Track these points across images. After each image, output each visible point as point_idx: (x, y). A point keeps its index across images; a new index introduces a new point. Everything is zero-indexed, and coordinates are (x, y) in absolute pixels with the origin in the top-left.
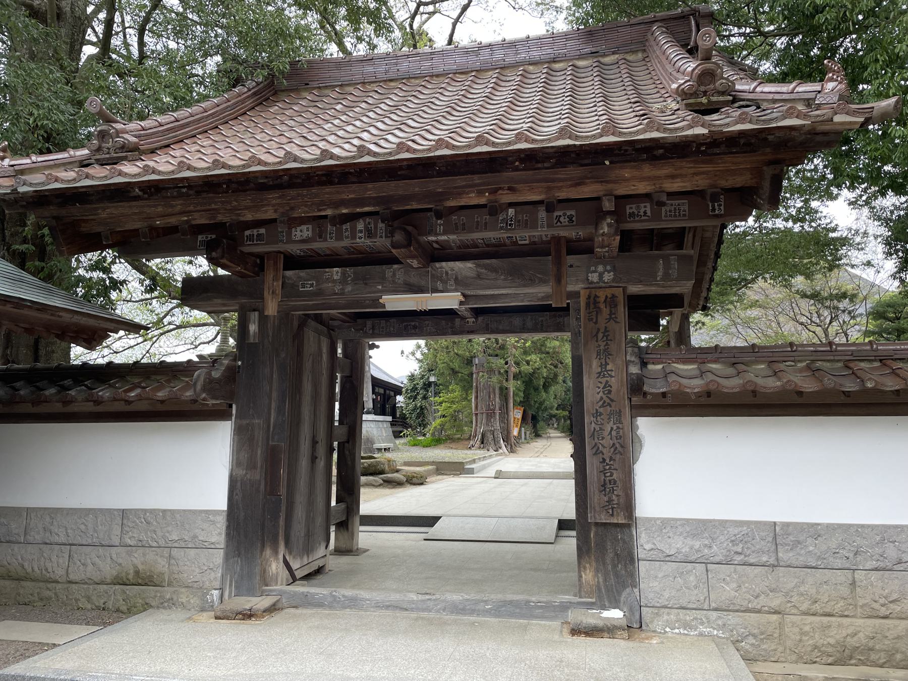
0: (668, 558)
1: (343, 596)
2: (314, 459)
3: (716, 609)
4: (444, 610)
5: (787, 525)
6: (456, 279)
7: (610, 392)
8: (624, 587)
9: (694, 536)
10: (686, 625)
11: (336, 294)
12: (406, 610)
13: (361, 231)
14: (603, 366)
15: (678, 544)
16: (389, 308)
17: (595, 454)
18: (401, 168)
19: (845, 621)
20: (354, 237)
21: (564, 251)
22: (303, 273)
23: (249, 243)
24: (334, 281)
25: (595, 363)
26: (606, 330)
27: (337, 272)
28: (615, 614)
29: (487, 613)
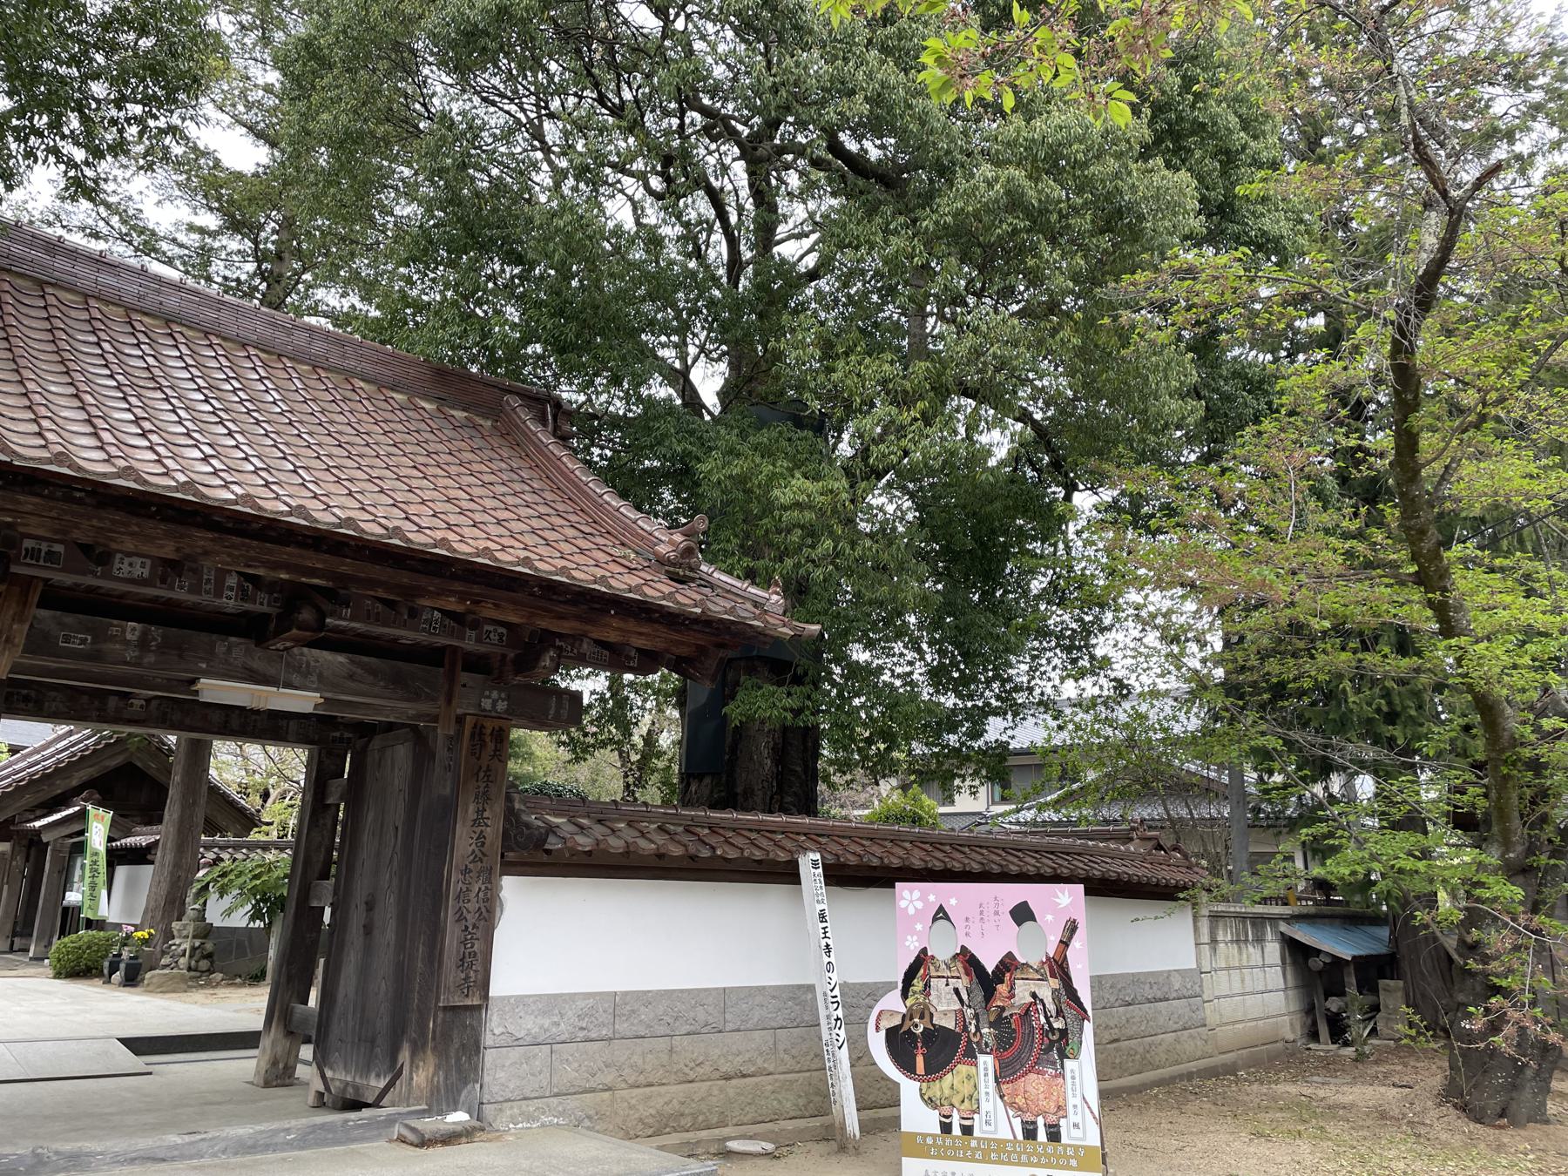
0: (517, 1042)
1: (57, 1153)
2: (368, 930)
3: (556, 1095)
4: (224, 1152)
5: (626, 993)
6: (320, 676)
7: (483, 844)
8: (466, 1084)
9: (544, 1013)
10: (529, 1118)
11: (126, 663)
12: (164, 1160)
13: (231, 589)
14: (480, 812)
15: (529, 1025)
16: (206, 697)
17: (458, 921)
18: (412, 558)
19: (662, 1089)
20: (219, 594)
21: (459, 667)
22: (70, 619)
23: (28, 561)
24: (126, 643)
25: (472, 808)
26: (488, 769)
27: (134, 629)
28: (459, 1117)
29: (290, 1145)
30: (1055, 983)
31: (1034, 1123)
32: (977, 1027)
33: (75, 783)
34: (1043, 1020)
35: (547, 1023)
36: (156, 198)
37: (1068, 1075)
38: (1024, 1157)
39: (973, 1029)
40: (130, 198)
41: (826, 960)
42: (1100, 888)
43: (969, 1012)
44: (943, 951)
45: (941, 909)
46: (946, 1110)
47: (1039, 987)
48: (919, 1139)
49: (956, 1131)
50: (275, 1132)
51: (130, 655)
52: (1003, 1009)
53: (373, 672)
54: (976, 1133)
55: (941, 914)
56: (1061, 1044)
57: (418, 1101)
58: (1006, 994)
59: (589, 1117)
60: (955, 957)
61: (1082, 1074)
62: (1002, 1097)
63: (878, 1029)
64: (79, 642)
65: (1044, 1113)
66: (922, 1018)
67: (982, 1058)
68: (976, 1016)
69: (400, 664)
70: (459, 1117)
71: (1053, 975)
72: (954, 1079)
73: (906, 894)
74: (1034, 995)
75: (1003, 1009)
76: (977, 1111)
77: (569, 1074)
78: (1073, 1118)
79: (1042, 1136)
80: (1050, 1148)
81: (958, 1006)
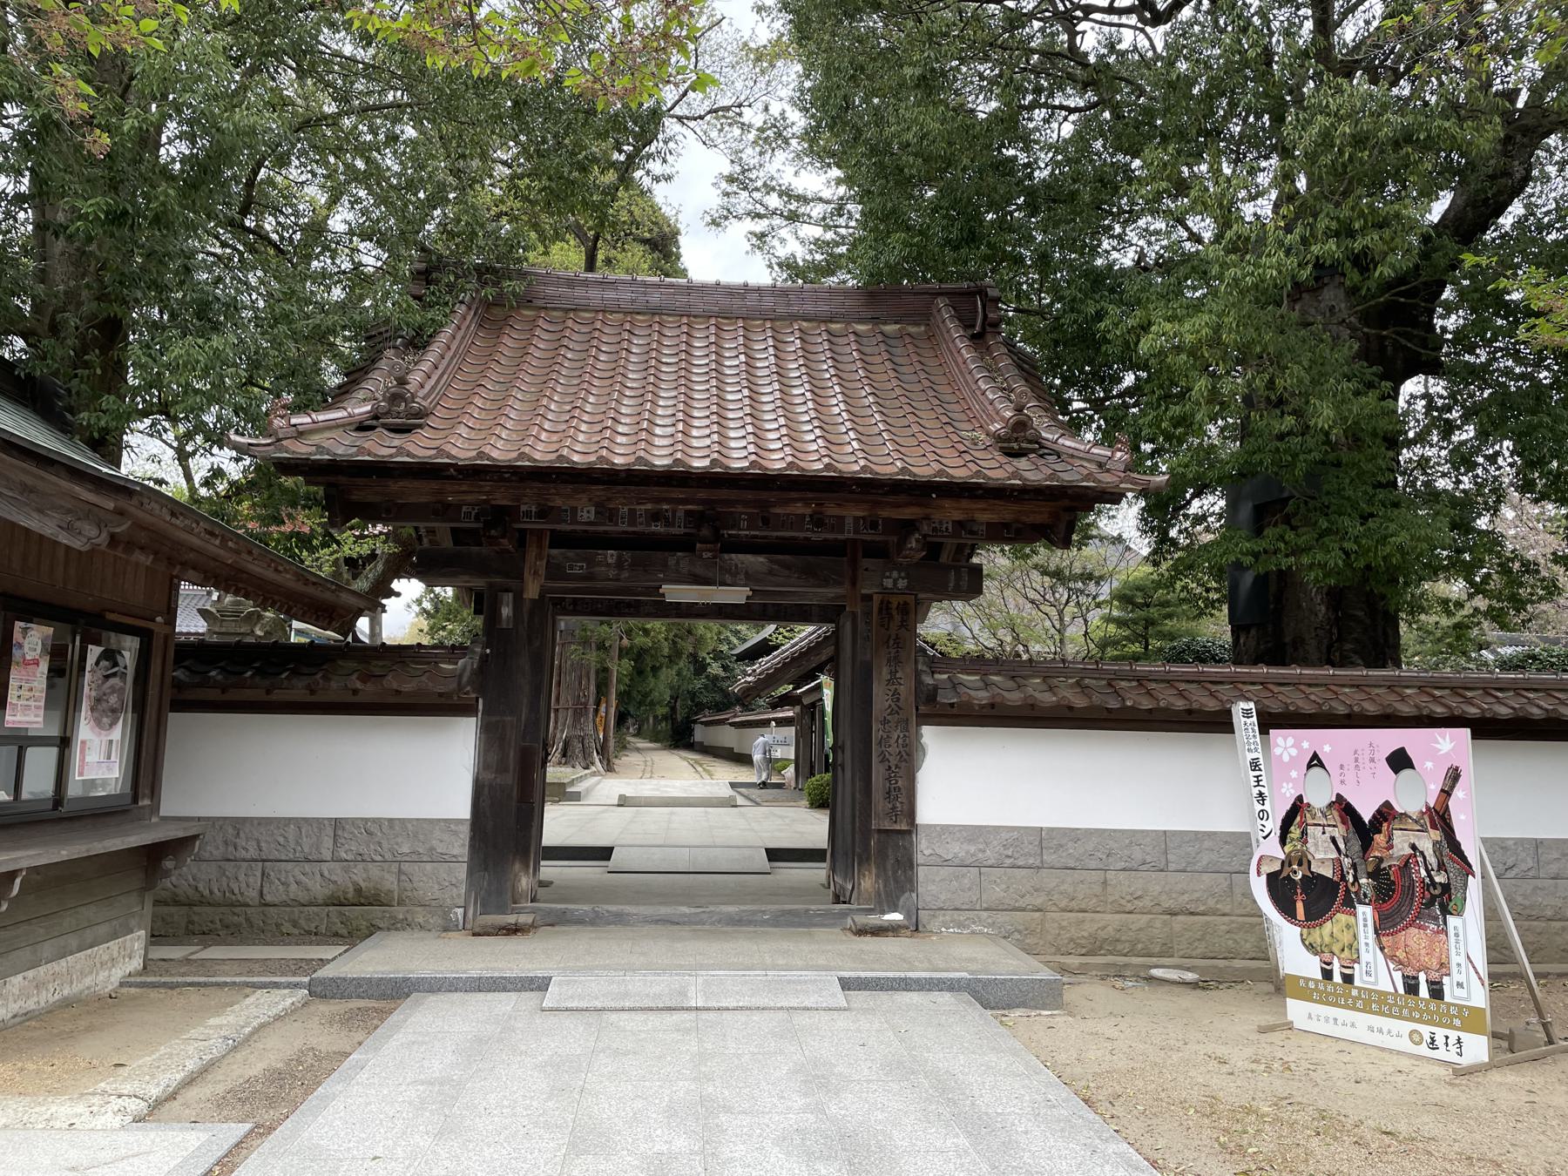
5: (1052, 830)
9: (970, 841)
10: (960, 925)
14: (893, 673)
15: (956, 849)
21: (860, 554)
22: (571, 553)
24: (608, 565)
25: (885, 670)
28: (896, 917)
29: (764, 923)
30: (1436, 835)
31: (1416, 978)
32: (1355, 877)
33: (824, 658)
34: (1423, 873)
35: (972, 849)
36: (793, 170)
37: (1451, 932)
38: (1405, 1012)
39: (1351, 878)
40: (772, 178)
41: (1258, 807)
42: (1486, 729)
43: (1347, 862)
44: (1319, 798)
45: (1315, 756)
46: (1327, 956)
47: (1419, 838)
48: (1302, 983)
49: (1337, 978)
50: (754, 913)
51: (612, 573)
52: (1381, 860)
53: (788, 567)
54: (1357, 982)
55: (1315, 761)
56: (1443, 900)
57: (868, 901)
58: (1384, 844)
59: (1020, 932)
60: (1331, 805)
61: (1466, 934)
62: (1382, 949)
63: (1259, 874)
64: (579, 568)
65: (1426, 969)
66: (1300, 864)
67: (1361, 909)
68: (1354, 866)
69: (810, 558)
70: (896, 917)
71: (1434, 827)
72: (1334, 927)
73: (1280, 741)
74: (1413, 847)
75: (1381, 860)
76: (1357, 961)
77: (996, 893)
78: (1456, 977)
79: (1424, 991)
80: (1433, 1006)
81: (1335, 855)
